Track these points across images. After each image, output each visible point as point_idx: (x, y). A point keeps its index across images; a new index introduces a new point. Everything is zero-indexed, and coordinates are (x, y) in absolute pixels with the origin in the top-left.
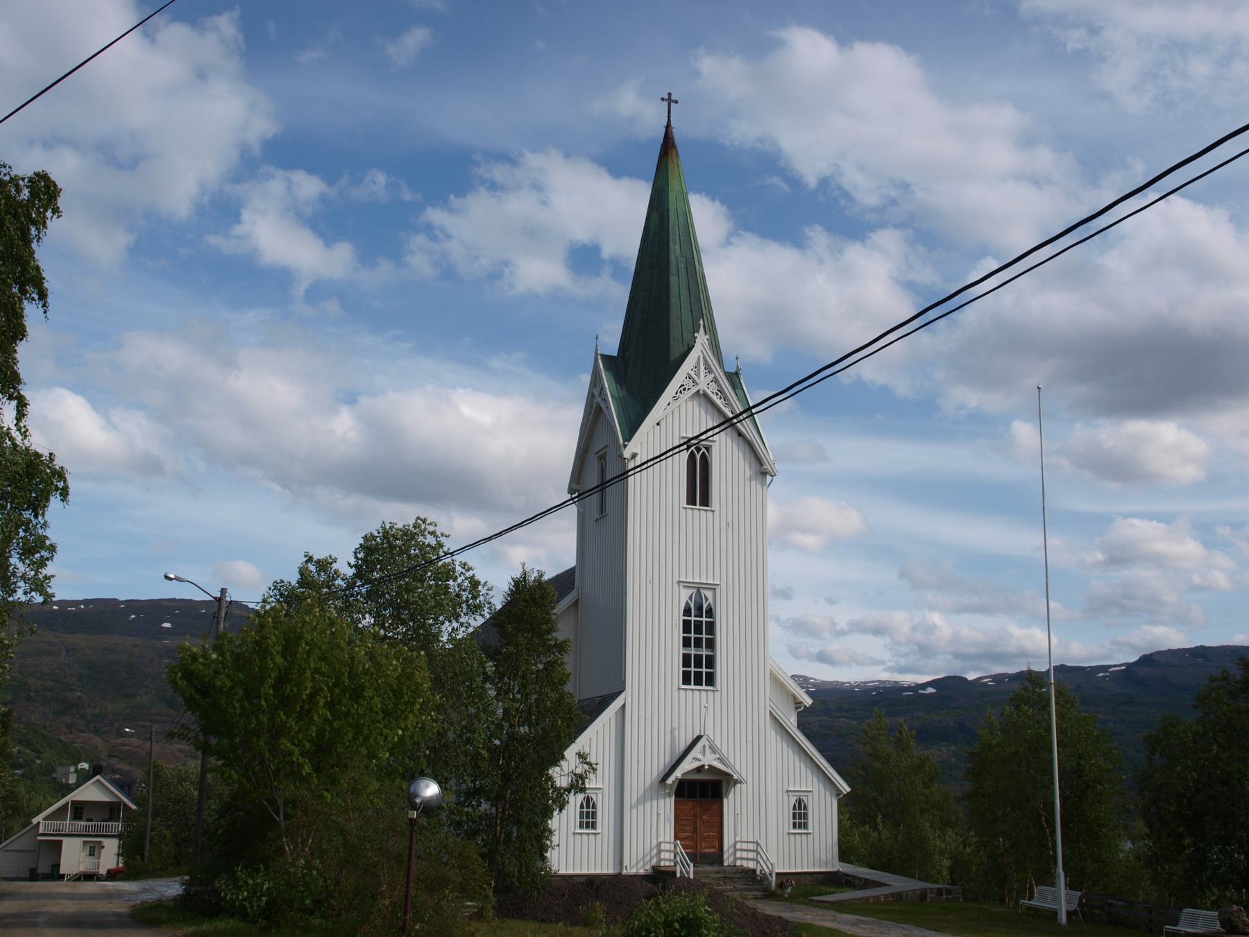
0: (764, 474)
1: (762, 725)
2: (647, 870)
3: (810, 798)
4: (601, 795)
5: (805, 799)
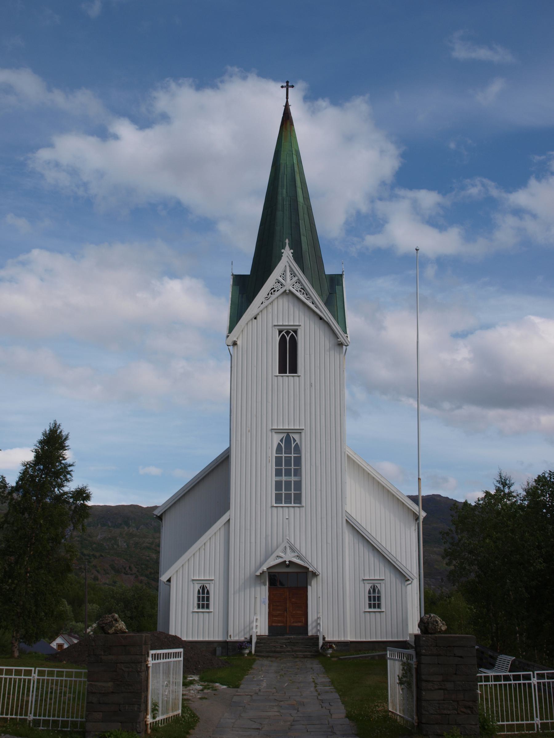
0: (341, 345)
1: (340, 531)
2: (246, 638)
3: (383, 585)
4: (384, 585)
5: (378, 585)
